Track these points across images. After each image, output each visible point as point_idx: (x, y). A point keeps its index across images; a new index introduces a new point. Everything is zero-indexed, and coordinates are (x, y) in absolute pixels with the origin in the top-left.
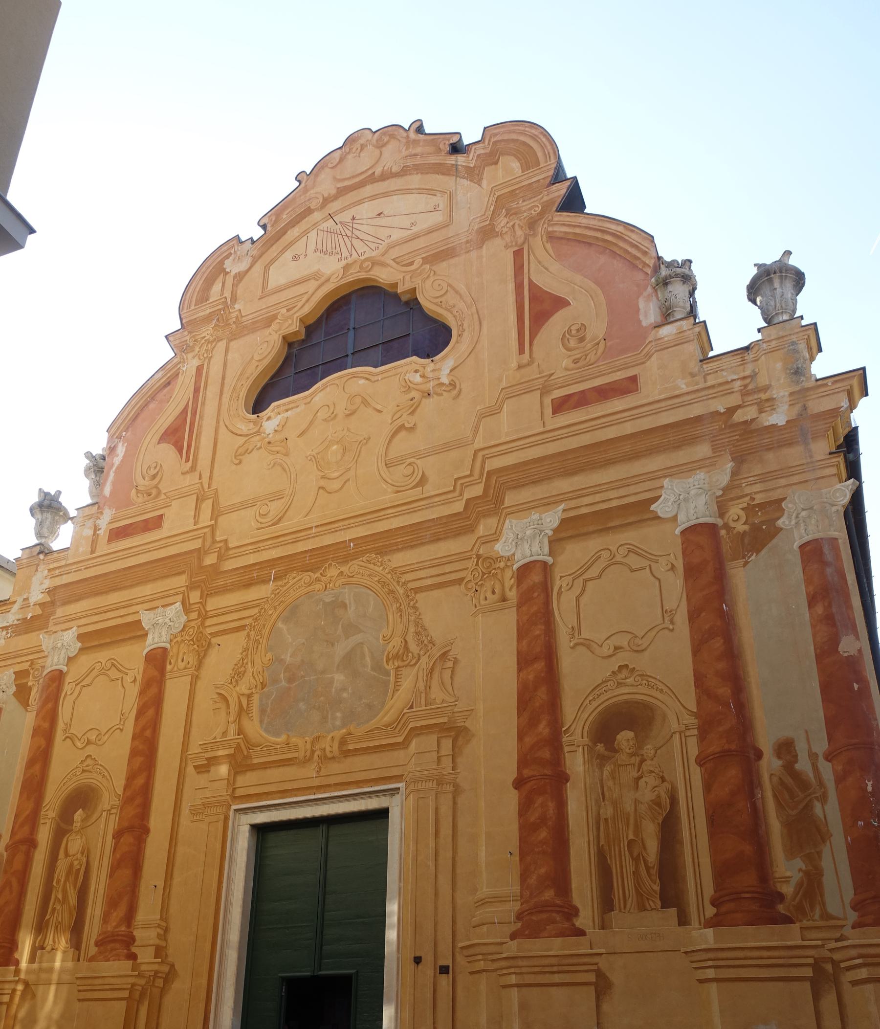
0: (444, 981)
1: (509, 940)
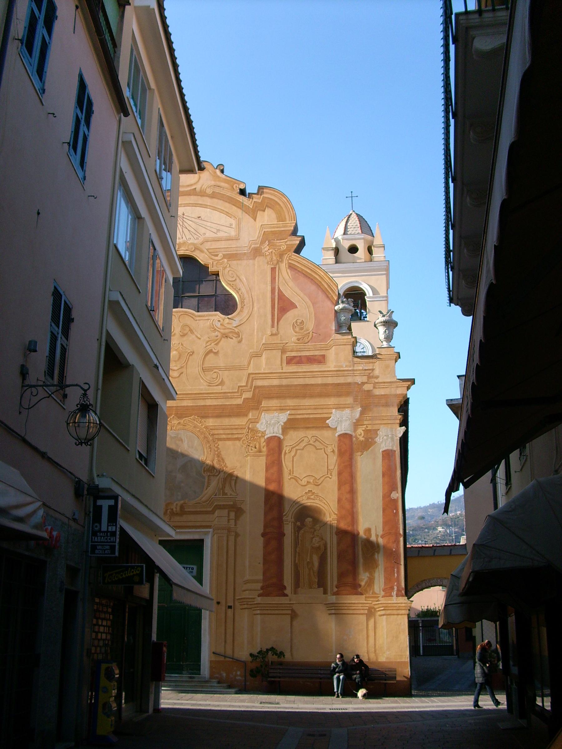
0: (230, 611)
1: (257, 597)
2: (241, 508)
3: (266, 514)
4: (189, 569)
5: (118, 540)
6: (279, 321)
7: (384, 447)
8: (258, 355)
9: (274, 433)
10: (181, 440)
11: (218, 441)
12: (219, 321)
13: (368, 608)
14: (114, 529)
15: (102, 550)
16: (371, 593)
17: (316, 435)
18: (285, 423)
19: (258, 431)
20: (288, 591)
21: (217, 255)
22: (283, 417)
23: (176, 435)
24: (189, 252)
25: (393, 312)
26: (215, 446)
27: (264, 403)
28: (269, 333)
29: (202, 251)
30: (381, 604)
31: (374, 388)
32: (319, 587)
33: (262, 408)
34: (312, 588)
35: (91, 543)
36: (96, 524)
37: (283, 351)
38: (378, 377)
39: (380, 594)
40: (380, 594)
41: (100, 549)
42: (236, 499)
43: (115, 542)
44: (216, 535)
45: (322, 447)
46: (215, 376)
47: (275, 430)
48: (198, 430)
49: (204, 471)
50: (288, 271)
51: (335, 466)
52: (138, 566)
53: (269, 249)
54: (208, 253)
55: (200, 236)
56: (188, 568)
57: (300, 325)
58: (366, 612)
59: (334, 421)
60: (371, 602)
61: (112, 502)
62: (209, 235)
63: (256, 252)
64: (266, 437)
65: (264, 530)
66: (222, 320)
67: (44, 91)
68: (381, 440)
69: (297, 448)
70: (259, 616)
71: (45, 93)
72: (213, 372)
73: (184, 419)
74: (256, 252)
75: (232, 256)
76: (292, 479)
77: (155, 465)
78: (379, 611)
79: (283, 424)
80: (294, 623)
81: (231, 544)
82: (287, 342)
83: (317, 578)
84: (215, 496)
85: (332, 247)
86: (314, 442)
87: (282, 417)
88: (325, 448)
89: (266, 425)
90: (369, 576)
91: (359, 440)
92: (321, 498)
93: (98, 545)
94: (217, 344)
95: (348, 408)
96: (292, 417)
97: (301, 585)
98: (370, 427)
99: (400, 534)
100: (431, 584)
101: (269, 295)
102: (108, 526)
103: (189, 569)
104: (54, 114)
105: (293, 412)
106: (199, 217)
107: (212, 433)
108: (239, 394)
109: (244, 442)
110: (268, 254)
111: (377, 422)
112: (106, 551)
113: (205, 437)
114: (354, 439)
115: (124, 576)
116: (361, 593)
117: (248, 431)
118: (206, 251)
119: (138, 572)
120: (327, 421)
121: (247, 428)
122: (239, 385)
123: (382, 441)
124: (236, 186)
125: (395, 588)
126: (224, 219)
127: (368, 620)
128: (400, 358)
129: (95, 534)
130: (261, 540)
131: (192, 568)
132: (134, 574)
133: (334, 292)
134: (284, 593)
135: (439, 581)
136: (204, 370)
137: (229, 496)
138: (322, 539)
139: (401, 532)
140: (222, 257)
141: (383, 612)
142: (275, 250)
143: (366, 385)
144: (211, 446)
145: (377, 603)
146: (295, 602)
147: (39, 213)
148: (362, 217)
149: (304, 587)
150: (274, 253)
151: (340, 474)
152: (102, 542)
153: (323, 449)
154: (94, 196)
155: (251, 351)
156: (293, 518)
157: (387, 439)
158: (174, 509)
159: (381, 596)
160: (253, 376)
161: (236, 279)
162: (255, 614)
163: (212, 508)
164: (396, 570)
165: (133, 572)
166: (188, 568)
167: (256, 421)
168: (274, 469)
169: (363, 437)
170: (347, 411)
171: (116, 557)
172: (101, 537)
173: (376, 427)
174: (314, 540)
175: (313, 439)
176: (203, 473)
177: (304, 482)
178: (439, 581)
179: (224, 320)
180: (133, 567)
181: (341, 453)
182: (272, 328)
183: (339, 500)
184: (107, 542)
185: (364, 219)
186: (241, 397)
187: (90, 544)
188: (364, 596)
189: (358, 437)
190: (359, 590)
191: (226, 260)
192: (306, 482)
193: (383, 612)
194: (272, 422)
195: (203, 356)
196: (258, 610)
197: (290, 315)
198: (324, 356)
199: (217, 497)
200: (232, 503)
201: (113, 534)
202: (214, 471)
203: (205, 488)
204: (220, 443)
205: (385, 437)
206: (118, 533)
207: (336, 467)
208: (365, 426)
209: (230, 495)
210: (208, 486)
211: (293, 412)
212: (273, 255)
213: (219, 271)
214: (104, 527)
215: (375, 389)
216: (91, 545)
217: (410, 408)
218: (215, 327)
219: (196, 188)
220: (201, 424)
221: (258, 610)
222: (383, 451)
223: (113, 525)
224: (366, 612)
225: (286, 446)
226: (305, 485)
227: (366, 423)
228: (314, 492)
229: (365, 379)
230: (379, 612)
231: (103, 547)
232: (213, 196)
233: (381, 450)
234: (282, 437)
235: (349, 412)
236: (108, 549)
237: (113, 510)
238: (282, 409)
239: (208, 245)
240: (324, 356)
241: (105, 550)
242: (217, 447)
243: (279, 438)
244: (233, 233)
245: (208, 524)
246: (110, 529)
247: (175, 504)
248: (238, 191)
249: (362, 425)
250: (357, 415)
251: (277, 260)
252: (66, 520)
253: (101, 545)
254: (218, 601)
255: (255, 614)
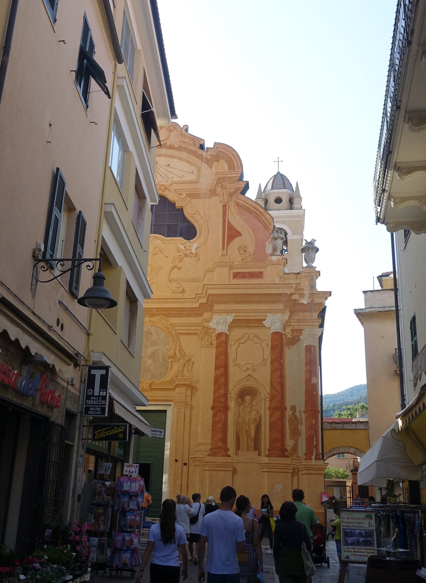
0: (185, 468)
2: (196, 387)
3: (215, 393)
4: (159, 432)
5: (107, 403)
6: (228, 246)
7: (306, 343)
8: (212, 271)
9: (222, 330)
10: (151, 334)
11: (180, 335)
12: (182, 244)
13: (292, 468)
14: (105, 394)
15: (94, 411)
16: (295, 456)
17: (255, 333)
18: (231, 323)
19: (211, 329)
20: (230, 452)
21: (182, 195)
22: (230, 318)
23: (147, 330)
24: (161, 191)
25: (316, 240)
26: (177, 338)
27: (216, 307)
28: (220, 254)
29: (169, 190)
30: (304, 465)
31: (300, 297)
32: (255, 450)
33: (214, 311)
34: (249, 451)
35: (85, 405)
36: (90, 390)
37: (231, 268)
38: (303, 290)
39: (303, 457)
40: (303, 457)
41: (92, 410)
42: (192, 380)
43: (105, 405)
44: (176, 407)
45: (259, 341)
46: (178, 285)
47: (223, 328)
48: (164, 326)
49: (168, 358)
50: (236, 208)
51: (269, 357)
52: (122, 426)
53: (221, 191)
54: (174, 192)
55: (169, 179)
56: (158, 432)
57: (243, 249)
58: (291, 471)
59: (269, 322)
60: (295, 463)
61: (103, 372)
62: (176, 179)
63: (213, 193)
64: (216, 333)
65: (213, 404)
66: (184, 244)
67: (56, 20)
68: (304, 338)
69: (240, 342)
70: (208, 472)
71: (57, 22)
72: (177, 283)
73: (154, 318)
74: (213, 193)
75: (194, 195)
76: (235, 366)
77: (135, 348)
78: (301, 471)
79: (229, 323)
80: (235, 478)
81: (188, 414)
82: (234, 261)
83: (253, 443)
84: (176, 377)
85: (262, 198)
86: (253, 338)
87: (229, 318)
88: (261, 342)
89: (216, 324)
90: (294, 442)
91: (288, 337)
92: (257, 381)
93: (91, 407)
94: (180, 262)
95: (279, 312)
96: (237, 318)
97: (241, 448)
98: (296, 328)
99: (319, 411)
100: (340, 451)
101: (221, 225)
102: (100, 391)
103: (159, 432)
104: (64, 41)
105: (237, 314)
106: (169, 165)
107: (175, 329)
108: (196, 300)
109: (199, 336)
110: (221, 194)
111: (303, 324)
112: (98, 412)
113: (170, 332)
114: (284, 336)
115: (111, 433)
116: (287, 455)
117: (203, 328)
118: (173, 191)
119: (122, 430)
120: (264, 322)
121: (202, 326)
122: (196, 293)
123: (305, 338)
124: (198, 142)
125: (314, 452)
126: (187, 167)
127: (292, 477)
128: (320, 276)
129: (88, 397)
130: (210, 413)
131: (161, 431)
132: (119, 432)
133: (270, 224)
134: (227, 453)
135: (347, 449)
136: (170, 281)
137: (187, 378)
138: (258, 413)
139: (320, 409)
140: (186, 196)
141: (305, 472)
142: (226, 192)
143: (294, 295)
144: (174, 339)
145: (300, 464)
146: (236, 462)
147: (50, 125)
148: (286, 177)
149: (243, 450)
150: (226, 194)
151: (272, 362)
152: (95, 405)
153: (260, 343)
154: (95, 123)
155: (206, 267)
156: (235, 395)
157: (309, 337)
158: (145, 387)
159: (303, 459)
160: (208, 286)
161: (196, 213)
162: (204, 470)
163: (174, 386)
164: (315, 438)
165: (118, 430)
166: (158, 432)
167: (209, 320)
168: (223, 357)
169: (291, 335)
170: (279, 315)
171: (106, 417)
172: (94, 400)
173: (301, 328)
174: (251, 413)
175: (253, 335)
176: (167, 359)
177: (244, 369)
178: (347, 449)
179: (186, 244)
180: (118, 426)
181: (273, 348)
182: (223, 250)
183: (272, 383)
184: (99, 405)
185: (287, 178)
186: (198, 302)
187: (85, 406)
188: (290, 458)
189: (287, 334)
190: (286, 453)
191: (188, 198)
192: (246, 368)
193: (305, 472)
194: (221, 321)
195: (170, 270)
196: (207, 466)
197: (236, 242)
198: (261, 273)
199: (178, 378)
200: (189, 383)
201: (104, 398)
202: (176, 358)
203: (169, 370)
204: (181, 336)
205: (308, 336)
206: (108, 397)
207: (270, 357)
208: (292, 327)
209: (188, 377)
210: (171, 370)
211: (237, 314)
212: (225, 195)
213: (183, 207)
214: (96, 393)
215: (300, 298)
216: (85, 406)
217: (326, 314)
218: (179, 248)
219: (166, 143)
220: (166, 322)
221: (207, 466)
222: (306, 346)
223: (104, 391)
224: (291, 471)
225: (232, 340)
226: (245, 371)
227: (293, 324)
228: (252, 376)
229: (292, 291)
230: (301, 472)
231: (95, 409)
232: (179, 149)
233: (304, 346)
234: (228, 333)
235: (280, 316)
236: (99, 411)
237: (104, 379)
238: (229, 312)
239: (175, 187)
240: (261, 273)
241: (96, 411)
242: (179, 340)
243: (227, 334)
244: (193, 177)
245: (170, 399)
246: (101, 394)
247: (145, 383)
248: (199, 146)
249: (290, 326)
250: (286, 318)
251: (228, 199)
252: (65, 385)
253: (93, 407)
254: (176, 459)
255: (204, 470)
